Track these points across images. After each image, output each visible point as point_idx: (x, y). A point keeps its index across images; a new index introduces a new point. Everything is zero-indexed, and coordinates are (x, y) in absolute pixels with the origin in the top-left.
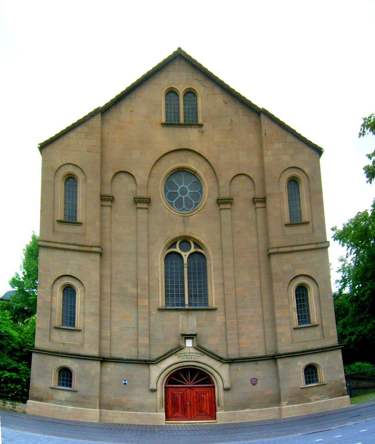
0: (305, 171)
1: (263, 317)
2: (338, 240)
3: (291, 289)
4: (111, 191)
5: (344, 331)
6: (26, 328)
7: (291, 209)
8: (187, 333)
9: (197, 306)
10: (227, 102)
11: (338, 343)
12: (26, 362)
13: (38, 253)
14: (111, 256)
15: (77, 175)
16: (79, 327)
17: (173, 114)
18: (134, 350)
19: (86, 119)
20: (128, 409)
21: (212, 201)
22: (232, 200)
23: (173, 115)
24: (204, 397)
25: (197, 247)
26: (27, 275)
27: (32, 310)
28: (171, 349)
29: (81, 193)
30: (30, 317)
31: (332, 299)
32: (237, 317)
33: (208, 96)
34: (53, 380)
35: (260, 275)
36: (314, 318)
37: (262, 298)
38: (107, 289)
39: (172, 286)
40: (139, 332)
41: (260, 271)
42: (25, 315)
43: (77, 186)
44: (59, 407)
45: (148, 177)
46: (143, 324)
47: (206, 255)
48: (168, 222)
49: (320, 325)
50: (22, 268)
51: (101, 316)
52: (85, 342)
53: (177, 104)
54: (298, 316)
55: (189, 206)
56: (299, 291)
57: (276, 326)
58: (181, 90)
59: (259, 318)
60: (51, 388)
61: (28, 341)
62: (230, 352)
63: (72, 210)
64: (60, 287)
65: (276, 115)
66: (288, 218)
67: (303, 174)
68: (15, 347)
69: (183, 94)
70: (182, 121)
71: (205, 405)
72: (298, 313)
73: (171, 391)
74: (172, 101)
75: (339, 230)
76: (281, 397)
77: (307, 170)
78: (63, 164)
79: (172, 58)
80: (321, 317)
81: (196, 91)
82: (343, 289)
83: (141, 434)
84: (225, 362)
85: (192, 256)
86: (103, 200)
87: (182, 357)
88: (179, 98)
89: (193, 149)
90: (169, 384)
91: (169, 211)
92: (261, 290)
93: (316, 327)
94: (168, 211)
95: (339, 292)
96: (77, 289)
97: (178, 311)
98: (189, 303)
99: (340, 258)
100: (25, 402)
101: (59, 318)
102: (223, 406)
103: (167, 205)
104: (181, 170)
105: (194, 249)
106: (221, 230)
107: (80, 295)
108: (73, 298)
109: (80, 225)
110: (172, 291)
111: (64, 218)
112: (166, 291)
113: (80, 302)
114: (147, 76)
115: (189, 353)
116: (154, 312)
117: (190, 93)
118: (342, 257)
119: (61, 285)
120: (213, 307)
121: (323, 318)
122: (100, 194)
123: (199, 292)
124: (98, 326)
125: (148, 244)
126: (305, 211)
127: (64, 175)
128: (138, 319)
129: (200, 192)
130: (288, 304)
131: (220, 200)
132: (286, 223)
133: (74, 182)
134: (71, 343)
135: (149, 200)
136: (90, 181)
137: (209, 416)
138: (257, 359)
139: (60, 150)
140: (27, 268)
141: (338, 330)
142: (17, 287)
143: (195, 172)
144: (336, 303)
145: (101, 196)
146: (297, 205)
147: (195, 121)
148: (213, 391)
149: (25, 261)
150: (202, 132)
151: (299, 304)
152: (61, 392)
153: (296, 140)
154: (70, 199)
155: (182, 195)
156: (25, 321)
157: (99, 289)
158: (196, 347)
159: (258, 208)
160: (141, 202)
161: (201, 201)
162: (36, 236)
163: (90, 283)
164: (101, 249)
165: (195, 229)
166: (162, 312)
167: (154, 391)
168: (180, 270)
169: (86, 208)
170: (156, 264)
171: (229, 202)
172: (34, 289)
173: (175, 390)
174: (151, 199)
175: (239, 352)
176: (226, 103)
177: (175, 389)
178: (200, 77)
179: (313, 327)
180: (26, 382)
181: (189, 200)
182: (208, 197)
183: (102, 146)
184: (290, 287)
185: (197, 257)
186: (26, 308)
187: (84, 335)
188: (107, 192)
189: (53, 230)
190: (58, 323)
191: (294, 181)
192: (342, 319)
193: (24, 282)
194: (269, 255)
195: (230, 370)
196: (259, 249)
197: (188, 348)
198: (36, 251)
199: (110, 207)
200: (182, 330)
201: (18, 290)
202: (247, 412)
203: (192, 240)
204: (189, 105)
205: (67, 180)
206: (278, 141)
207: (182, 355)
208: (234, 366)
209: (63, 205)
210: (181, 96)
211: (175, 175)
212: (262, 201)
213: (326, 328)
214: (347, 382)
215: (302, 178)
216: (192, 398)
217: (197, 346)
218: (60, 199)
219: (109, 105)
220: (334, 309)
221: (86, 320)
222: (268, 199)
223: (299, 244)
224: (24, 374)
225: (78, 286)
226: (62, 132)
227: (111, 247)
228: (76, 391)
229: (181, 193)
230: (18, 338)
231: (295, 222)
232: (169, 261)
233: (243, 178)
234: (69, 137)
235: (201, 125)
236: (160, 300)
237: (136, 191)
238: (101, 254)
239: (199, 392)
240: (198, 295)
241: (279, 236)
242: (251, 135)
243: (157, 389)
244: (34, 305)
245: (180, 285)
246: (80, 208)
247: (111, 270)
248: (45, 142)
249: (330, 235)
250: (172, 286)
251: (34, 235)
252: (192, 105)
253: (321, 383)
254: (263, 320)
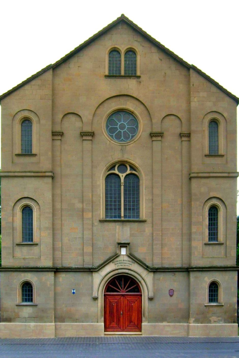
0: (224, 116)
1: (182, 231)
4: (61, 128)
7: (211, 144)
8: (122, 242)
9: (130, 218)
10: (162, 59)
11: (236, 265)
14: (61, 179)
15: (32, 118)
16: (37, 241)
17: (115, 68)
18: (80, 258)
19: (40, 74)
20: (76, 320)
22: (162, 134)
23: (115, 69)
24: (134, 305)
25: (132, 169)
29: (35, 132)
32: (162, 229)
33: (145, 54)
35: (182, 194)
36: (221, 237)
37: (182, 214)
38: (58, 206)
39: (111, 201)
41: (182, 191)
43: (32, 126)
45: (92, 116)
46: (87, 234)
47: (139, 175)
48: (109, 150)
51: (53, 229)
52: (41, 255)
53: (119, 61)
55: (127, 138)
56: (212, 211)
57: (191, 240)
58: (123, 49)
59: (179, 231)
64: (20, 208)
65: (203, 70)
66: (207, 151)
67: (222, 118)
69: (124, 53)
70: (123, 73)
71: (134, 314)
72: (209, 230)
73: (109, 298)
76: (190, 313)
77: (225, 115)
78: (19, 110)
79: (116, 23)
83: (86, 348)
84: (150, 270)
85: (128, 176)
87: (118, 265)
88: (120, 56)
89: (131, 95)
90: (107, 292)
91: (110, 141)
92: (182, 207)
93: (221, 245)
94: (109, 142)
96: (33, 208)
98: (124, 215)
101: (20, 235)
102: (147, 317)
103: (108, 137)
104: (121, 110)
105: (130, 171)
106: (152, 157)
109: (35, 156)
110: (111, 205)
112: (106, 205)
113: (37, 218)
115: (124, 261)
116: (96, 223)
117: (131, 52)
119: (21, 206)
121: (227, 238)
122: (51, 131)
123: (133, 206)
124: (52, 239)
125: (92, 168)
127: (20, 119)
129: (136, 128)
130: (203, 221)
131: (153, 133)
132: (205, 154)
133: (29, 123)
135: (93, 133)
136: (43, 122)
143: (133, 112)
145: (52, 132)
146: (216, 140)
148: (140, 300)
150: (139, 82)
151: (210, 222)
152: (24, 308)
155: (121, 130)
157: (51, 206)
158: (129, 255)
160: (86, 135)
161: (137, 134)
163: (44, 202)
164: (53, 174)
165: (131, 155)
166: (102, 223)
167: (95, 299)
168: (118, 188)
170: (98, 183)
174: (95, 133)
175: (162, 261)
176: (161, 60)
178: (140, 39)
181: (127, 133)
182: (142, 132)
183: (53, 94)
184: (205, 206)
185: (132, 177)
187: (41, 249)
188: (58, 129)
189: (12, 162)
190: (19, 240)
191: (214, 123)
194: (190, 178)
195: (154, 279)
196: (182, 173)
197: (123, 256)
200: (118, 239)
202: (164, 326)
203: (128, 164)
205: (23, 122)
207: (117, 263)
210: (123, 54)
212: (187, 136)
215: (221, 121)
216: (124, 306)
217: (130, 254)
218: (17, 138)
220: (237, 231)
221: (42, 234)
222: (192, 135)
223: (215, 172)
226: (18, 85)
227: (61, 171)
229: (120, 128)
231: (213, 154)
233: (173, 117)
235: (139, 77)
236: (102, 213)
237: (82, 127)
238: (53, 178)
240: (132, 208)
241: (199, 164)
242: (181, 85)
243: (98, 297)
245: (118, 200)
247: (61, 190)
250: (111, 201)
254: (182, 233)
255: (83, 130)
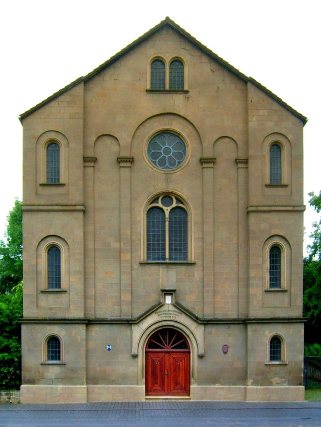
2: (314, 205)
3: (266, 249)
4: (94, 152)
5: (309, 302)
6: (14, 297)
8: (167, 289)
9: (176, 260)
10: (214, 70)
11: (303, 316)
12: (16, 337)
13: (21, 217)
16: (65, 287)
18: (117, 308)
19: (68, 89)
20: (112, 382)
21: (196, 160)
22: (215, 160)
23: (158, 82)
24: (180, 364)
25: (179, 202)
26: (12, 241)
27: (18, 276)
28: (151, 306)
30: (17, 284)
31: (302, 264)
32: (214, 273)
33: (194, 64)
34: (42, 354)
35: (238, 231)
36: (285, 283)
37: (238, 255)
38: (91, 246)
39: (154, 240)
40: (122, 288)
42: (12, 284)
44: (50, 387)
45: (131, 138)
46: (125, 279)
47: (187, 209)
48: (151, 179)
49: (289, 291)
50: (7, 235)
51: (85, 273)
52: (71, 304)
53: (163, 72)
54: (270, 278)
55: (172, 164)
56: (273, 252)
57: (249, 286)
59: (234, 276)
60: (41, 364)
61: (17, 312)
62: (206, 312)
63: (54, 173)
64: (45, 248)
66: (268, 180)
67: (286, 140)
68: (5, 321)
69: (169, 63)
70: (167, 87)
71: (181, 375)
73: (151, 356)
74: (158, 69)
75: (316, 196)
77: (290, 137)
78: (44, 132)
80: (291, 283)
81: (183, 60)
82: (314, 256)
84: (200, 322)
85: (173, 210)
86: (86, 161)
87: (162, 316)
88: (165, 66)
90: (149, 348)
91: (152, 169)
92: (238, 247)
93: (285, 292)
95: (309, 258)
97: (159, 264)
98: (169, 257)
99: (314, 224)
100: (18, 388)
102: (197, 379)
105: (176, 204)
106: (203, 187)
107: (65, 254)
108: (58, 257)
109: (63, 186)
110: (153, 245)
111: (47, 181)
112: (148, 245)
113: (65, 261)
114: (132, 46)
115: (168, 311)
116: (136, 266)
117: (177, 62)
118: (316, 222)
119: (46, 246)
120: (192, 261)
123: (180, 246)
124: (83, 285)
125: (131, 200)
126: (285, 174)
128: (120, 274)
130: (263, 263)
131: (203, 159)
133: (56, 147)
134: (58, 306)
135: (132, 159)
136: (72, 145)
137: (184, 391)
138: (230, 322)
139: (41, 118)
140: (11, 235)
141: (304, 300)
142: (3, 254)
143: (179, 134)
144: (305, 269)
145: (84, 158)
147: (180, 87)
148: (188, 357)
149: (9, 227)
150: (187, 98)
151: (272, 265)
152: (51, 368)
153: (281, 108)
154: (52, 163)
156: (12, 290)
157: (82, 246)
158: (175, 304)
159: (240, 168)
160: (124, 161)
161: (185, 160)
162: (20, 201)
163: (74, 241)
165: (177, 185)
167: (135, 356)
169: (69, 170)
170: (138, 218)
171: (212, 161)
172: (19, 254)
173: (155, 355)
174: (134, 159)
176: (213, 71)
177: (155, 354)
178: (188, 46)
179: (282, 292)
180: (18, 361)
181: (172, 159)
182: (191, 157)
183: (85, 113)
184: (266, 246)
185: (178, 212)
186: (12, 275)
187: (70, 297)
189: (36, 193)
191: (276, 147)
192: (308, 288)
193: (9, 249)
194: (248, 213)
195: (204, 333)
197: (167, 305)
198: (20, 216)
199: (93, 168)
200: (162, 286)
201: (4, 258)
202: (217, 389)
203: (174, 196)
204: (176, 73)
205: (49, 146)
206: (264, 109)
207: (161, 313)
208: (213, 329)
209: (45, 170)
211: (159, 137)
212: (244, 162)
213: (292, 301)
214: (305, 367)
215: (284, 144)
216: (169, 365)
218: (42, 164)
219: (92, 75)
221: (71, 279)
222: (250, 161)
223: (277, 205)
224: (16, 351)
225: (62, 245)
227: (94, 204)
228: (65, 364)
229: (164, 153)
230: (6, 310)
231: (275, 184)
232: (151, 215)
233: (227, 140)
234: (51, 106)
235: (187, 92)
236: (142, 254)
237: (120, 152)
238: (84, 212)
239: (176, 359)
240: (178, 249)
241: (259, 196)
243: (138, 355)
244: (21, 271)
246: (63, 170)
248: (26, 112)
249: (307, 199)
251: (17, 201)
252: (178, 73)
253: (283, 362)
254: (238, 278)
255: (121, 155)
